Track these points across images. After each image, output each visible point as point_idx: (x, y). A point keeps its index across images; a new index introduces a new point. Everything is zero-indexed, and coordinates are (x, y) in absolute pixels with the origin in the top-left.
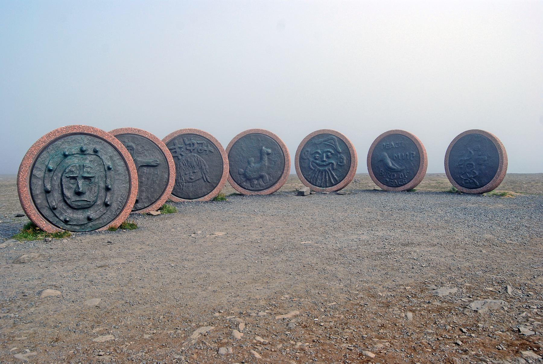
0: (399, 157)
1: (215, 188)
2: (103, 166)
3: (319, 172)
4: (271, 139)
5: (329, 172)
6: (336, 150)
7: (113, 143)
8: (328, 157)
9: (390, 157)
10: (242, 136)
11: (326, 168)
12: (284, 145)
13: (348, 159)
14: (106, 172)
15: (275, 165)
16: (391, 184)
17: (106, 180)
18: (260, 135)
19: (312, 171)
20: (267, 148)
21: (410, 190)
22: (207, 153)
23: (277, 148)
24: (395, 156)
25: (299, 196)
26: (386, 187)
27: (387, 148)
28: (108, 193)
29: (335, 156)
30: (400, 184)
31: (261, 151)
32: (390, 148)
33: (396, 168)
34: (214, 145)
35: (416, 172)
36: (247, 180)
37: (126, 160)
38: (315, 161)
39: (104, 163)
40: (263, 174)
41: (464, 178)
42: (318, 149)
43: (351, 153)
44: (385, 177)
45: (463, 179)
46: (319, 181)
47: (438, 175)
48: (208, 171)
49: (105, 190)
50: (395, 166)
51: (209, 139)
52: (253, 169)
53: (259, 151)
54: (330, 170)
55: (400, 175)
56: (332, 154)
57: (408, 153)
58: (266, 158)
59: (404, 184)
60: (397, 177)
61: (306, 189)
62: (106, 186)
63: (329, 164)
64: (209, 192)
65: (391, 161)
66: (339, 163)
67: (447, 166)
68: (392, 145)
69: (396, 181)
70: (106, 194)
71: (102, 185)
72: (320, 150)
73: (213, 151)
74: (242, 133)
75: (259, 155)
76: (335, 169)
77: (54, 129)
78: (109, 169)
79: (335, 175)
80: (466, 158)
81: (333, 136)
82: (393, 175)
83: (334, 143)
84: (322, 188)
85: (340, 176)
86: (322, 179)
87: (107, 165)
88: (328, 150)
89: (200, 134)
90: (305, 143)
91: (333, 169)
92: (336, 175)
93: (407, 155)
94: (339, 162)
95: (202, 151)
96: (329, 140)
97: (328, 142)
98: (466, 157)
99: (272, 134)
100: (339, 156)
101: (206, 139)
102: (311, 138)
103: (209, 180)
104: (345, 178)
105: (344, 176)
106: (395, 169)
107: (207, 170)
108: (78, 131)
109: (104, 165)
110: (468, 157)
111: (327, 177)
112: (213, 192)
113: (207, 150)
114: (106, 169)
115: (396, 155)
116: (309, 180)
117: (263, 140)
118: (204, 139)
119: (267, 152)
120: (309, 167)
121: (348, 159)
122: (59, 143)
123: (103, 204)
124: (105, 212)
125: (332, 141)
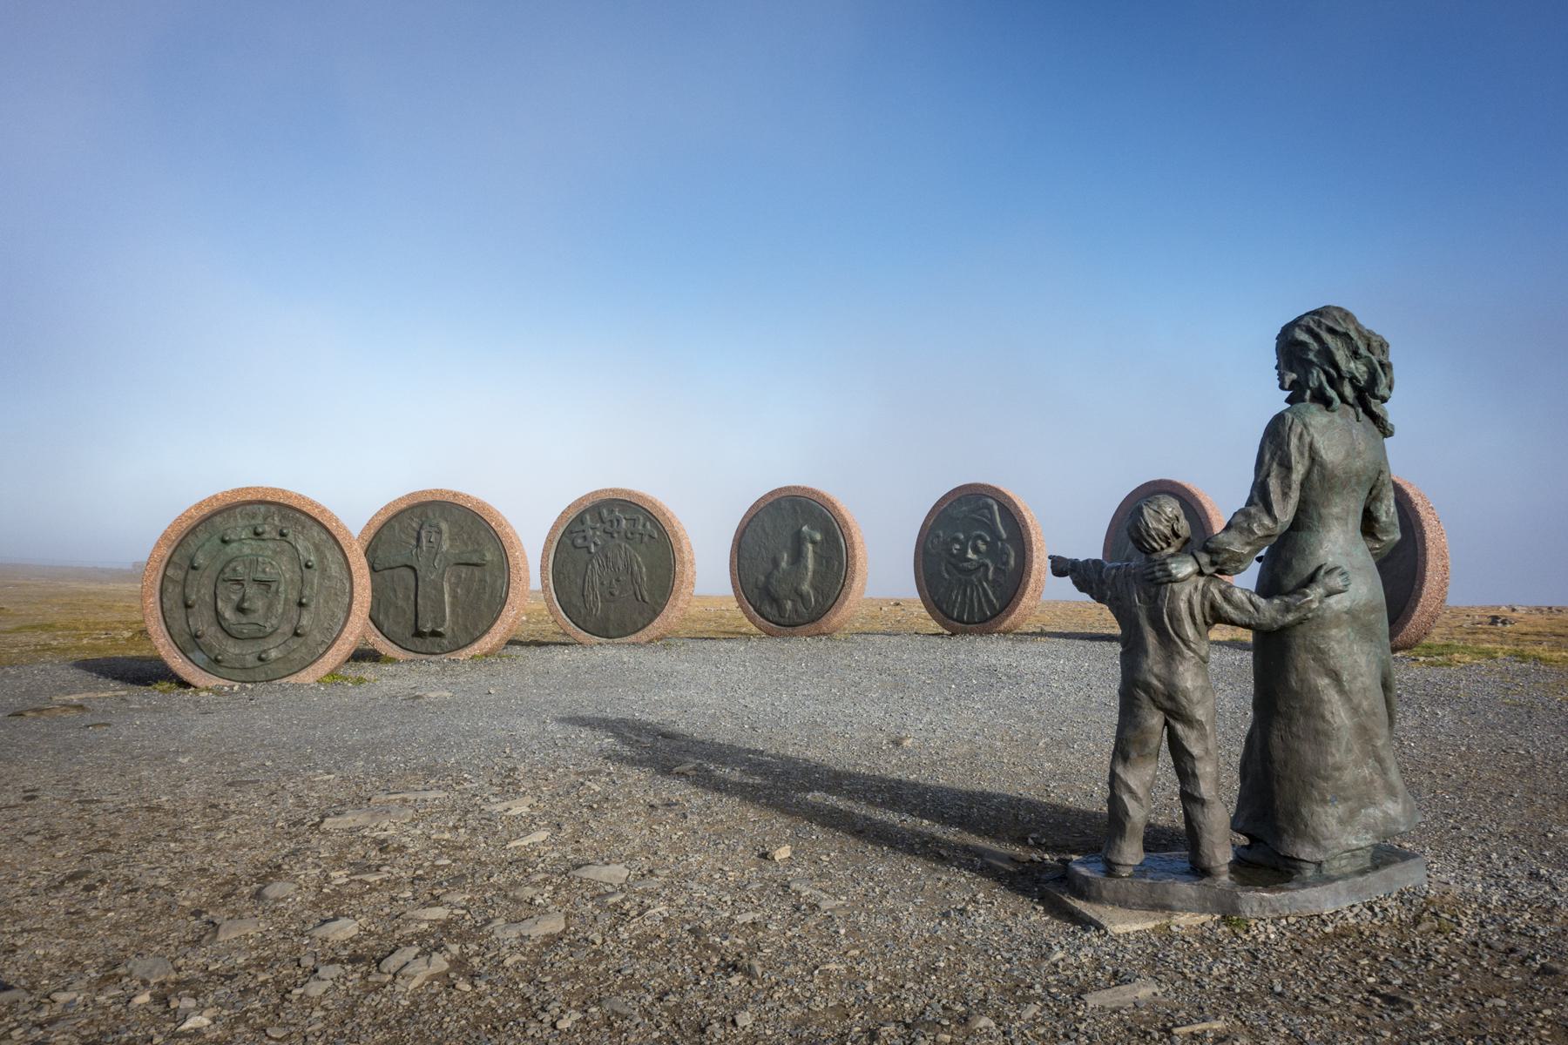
12: (846, 522)
28: (305, 613)
71: (294, 596)
77: (212, 494)
108: (254, 498)
122: (218, 519)
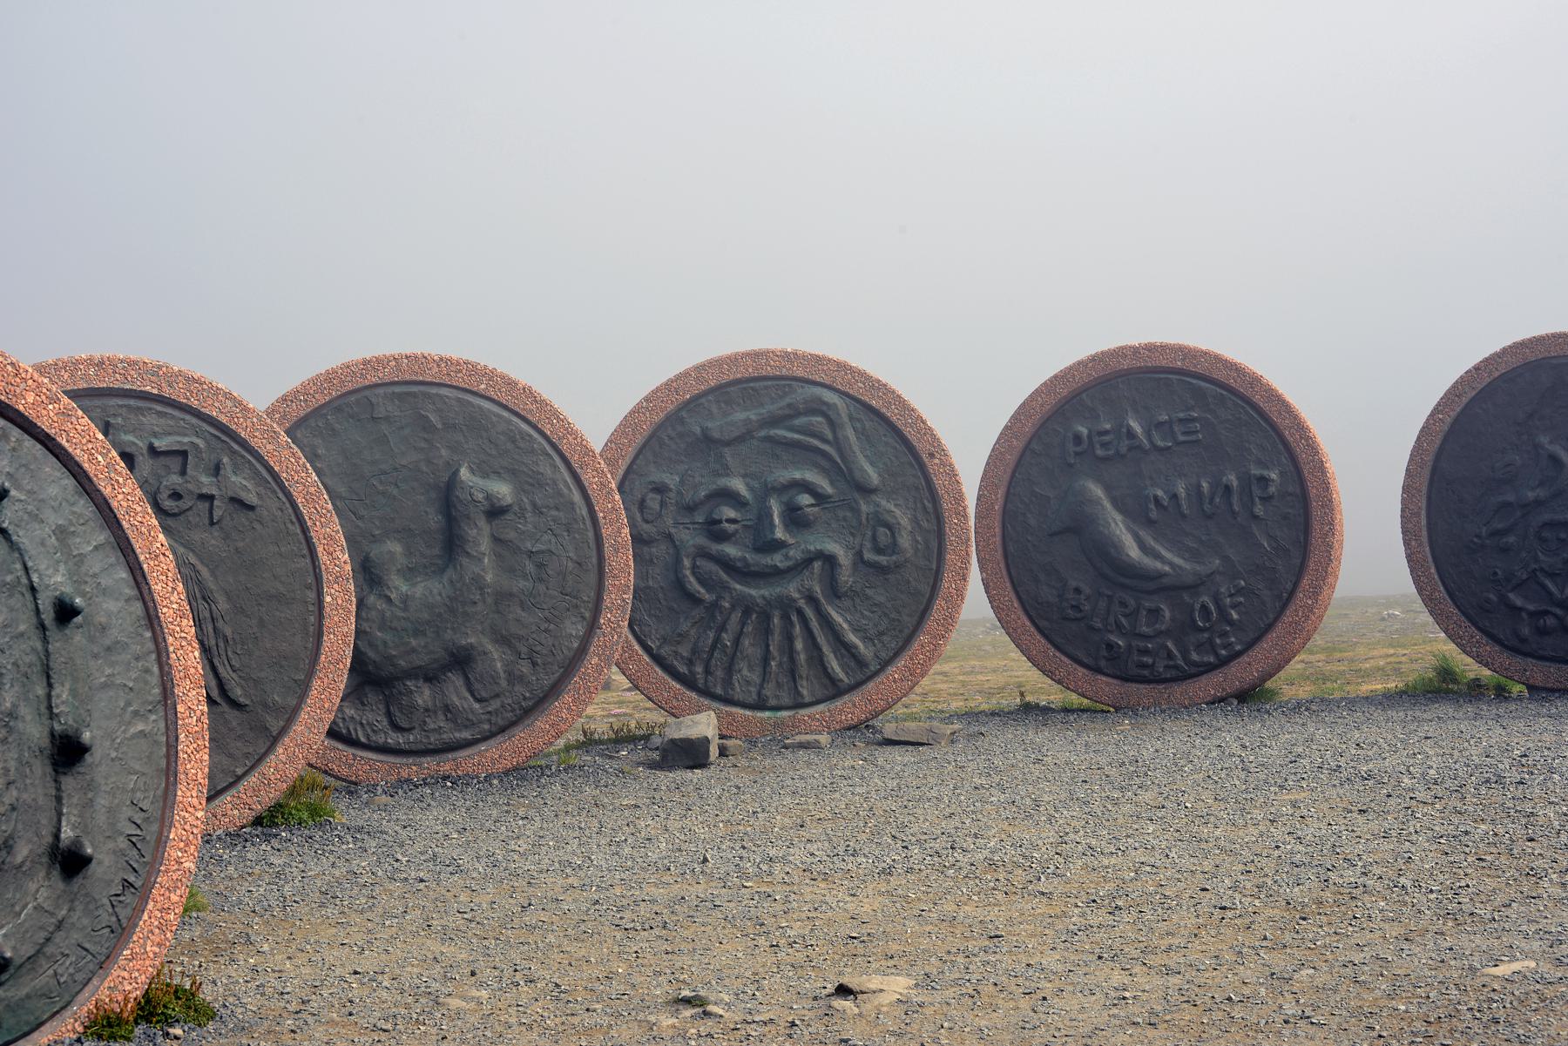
0: (1179, 506)
1: (274, 741)
2: (28, 596)
3: (747, 612)
4: (505, 414)
5: (809, 613)
6: (842, 471)
7: (64, 443)
8: (795, 518)
9: (1118, 504)
10: (314, 404)
11: (792, 589)
13: (925, 524)
14: (45, 641)
15: (541, 580)
16: (1144, 666)
17: (49, 696)
18: (434, 390)
19: (698, 612)
20: (485, 476)
21: (1250, 697)
22: (217, 514)
23: (548, 472)
24: (1157, 500)
25: (671, 768)
26: (1108, 684)
27: (1100, 452)
29: (841, 514)
30: (1195, 664)
31: (448, 498)
32: (1123, 450)
33: (1167, 568)
34: (259, 458)
35: (1289, 586)
36: (367, 689)
37: (138, 551)
38: (715, 548)
39: (35, 578)
40: (472, 640)
41: (1531, 607)
42: (727, 471)
43: (941, 492)
44: (1099, 625)
45: (1524, 615)
46: (745, 672)
47: (1390, 603)
48: (228, 631)
49: (47, 762)
50: (1158, 556)
51: (223, 419)
52: (405, 609)
53: (433, 495)
54: (812, 600)
55: (1197, 606)
56: (820, 498)
57: (1232, 479)
58: (480, 536)
59: (1223, 662)
60: (1173, 620)
61: (703, 724)
62: (52, 734)
63: (808, 562)
64: (239, 771)
65: (1129, 529)
66: (869, 555)
67: (1420, 545)
68: (1131, 434)
69: (1170, 644)
70: (58, 789)
72: (744, 476)
73: (252, 499)
74: (313, 381)
75: (434, 520)
76: (845, 594)
78: (65, 612)
79: (845, 626)
80: (1531, 495)
81: (818, 391)
82: (1150, 611)
83: (829, 435)
84: (767, 714)
85: (882, 634)
86: (766, 660)
87: (47, 586)
88: (797, 475)
89: (167, 392)
90: (639, 440)
91: (835, 592)
92: (855, 630)
93: (1228, 489)
94: (868, 545)
95: (185, 504)
96: (798, 414)
97: (792, 429)
98: (1533, 489)
99: (511, 384)
100: (864, 508)
101: (206, 427)
102: (679, 409)
103: (237, 693)
104: (916, 645)
105: (907, 631)
106: (1161, 575)
107: (220, 624)
109: (33, 589)
110: (1541, 484)
111: (799, 645)
112: (271, 766)
113: (214, 492)
114: (48, 617)
115: (1160, 493)
116: (683, 669)
117: (454, 426)
118: (194, 421)
119: (488, 497)
120: (680, 584)
121: (925, 524)
123: (45, 860)
124: (64, 912)
125: (820, 419)
